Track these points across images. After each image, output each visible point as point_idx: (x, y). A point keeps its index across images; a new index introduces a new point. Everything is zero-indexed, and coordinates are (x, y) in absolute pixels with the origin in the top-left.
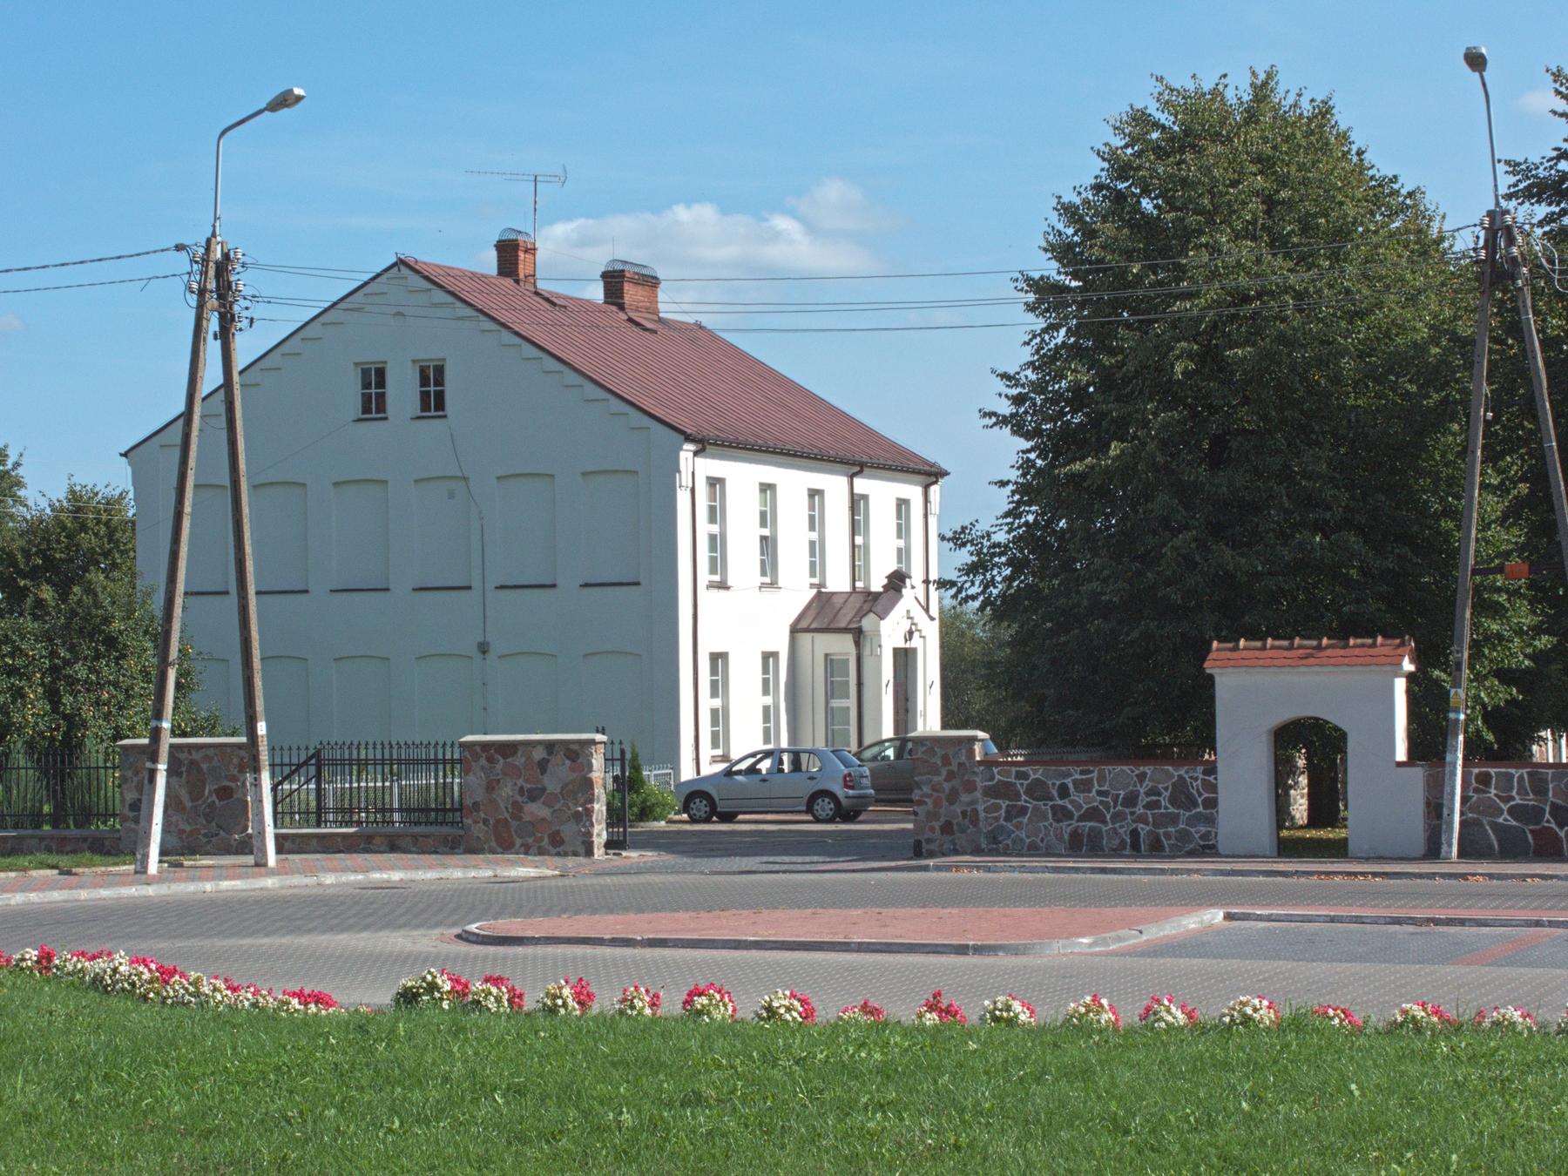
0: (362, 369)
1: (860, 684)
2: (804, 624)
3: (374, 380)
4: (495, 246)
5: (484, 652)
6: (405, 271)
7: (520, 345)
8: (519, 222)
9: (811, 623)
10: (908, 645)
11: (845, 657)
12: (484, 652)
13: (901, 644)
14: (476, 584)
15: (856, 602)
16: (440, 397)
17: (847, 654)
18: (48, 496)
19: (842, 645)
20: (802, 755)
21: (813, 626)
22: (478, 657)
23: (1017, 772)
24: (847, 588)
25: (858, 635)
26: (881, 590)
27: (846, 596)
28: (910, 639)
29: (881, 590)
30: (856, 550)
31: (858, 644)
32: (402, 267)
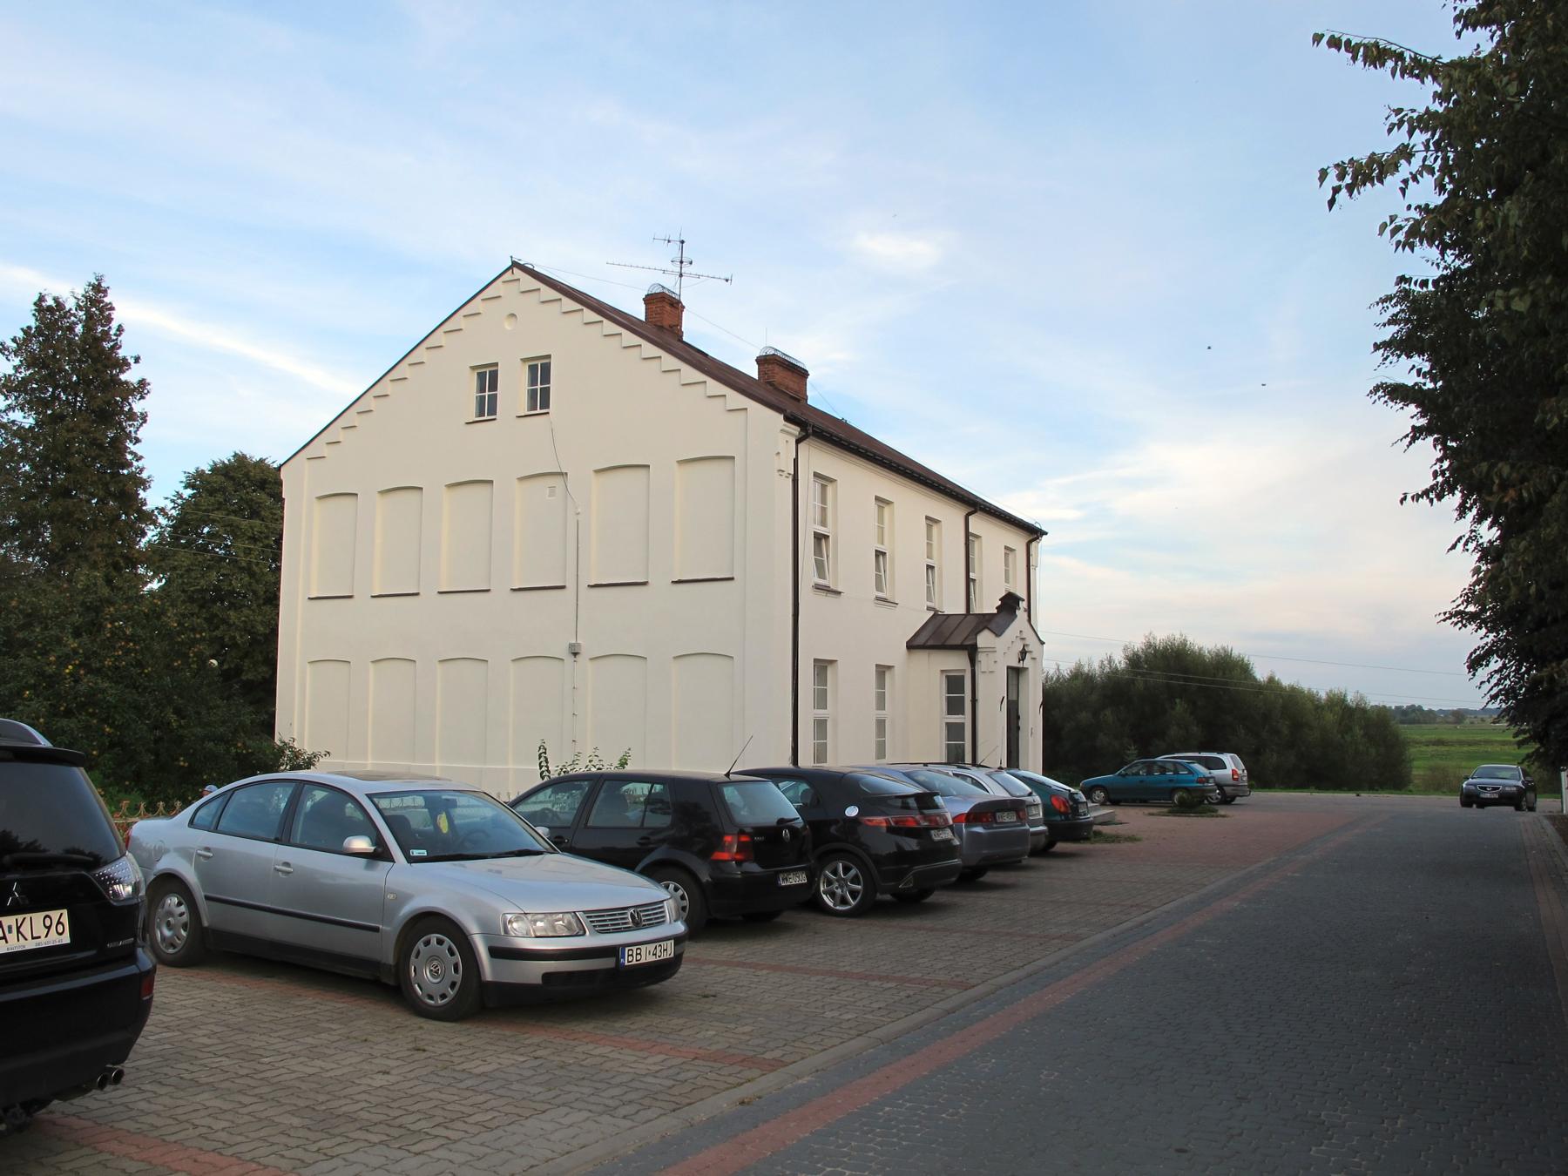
0: (478, 374)
1: (974, 701)
2: (921, 641)
3: (488, 378)
4: (644, 299)
5: (575, 654)
6: (518, 273)
7: (582, 310)
8: (670, 284)
9: (927, 641)
10: (1020, 665)
11: (1030, 763)
12: (575, 654)
13: (1015, 664)
14: (571, 584)
15: (970, 624)
16: (546, 393)
17: (965, 670)
18: (886, 713)
19: (956, 662)
20: (970, 762)
21: (929, 643)
22: (569, 659)
23: (962, 725)
24: (962, 611)
25: (972, 652)
26: (996, 611)
27: (962, 618)
28: (1023, 660)
29: (996, 611)
30: (971, 584)
31: (973, 661)
32: (515, 269)
